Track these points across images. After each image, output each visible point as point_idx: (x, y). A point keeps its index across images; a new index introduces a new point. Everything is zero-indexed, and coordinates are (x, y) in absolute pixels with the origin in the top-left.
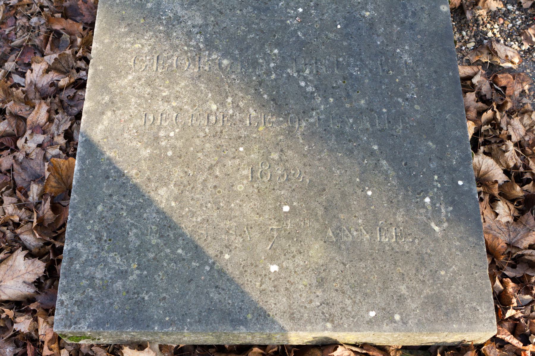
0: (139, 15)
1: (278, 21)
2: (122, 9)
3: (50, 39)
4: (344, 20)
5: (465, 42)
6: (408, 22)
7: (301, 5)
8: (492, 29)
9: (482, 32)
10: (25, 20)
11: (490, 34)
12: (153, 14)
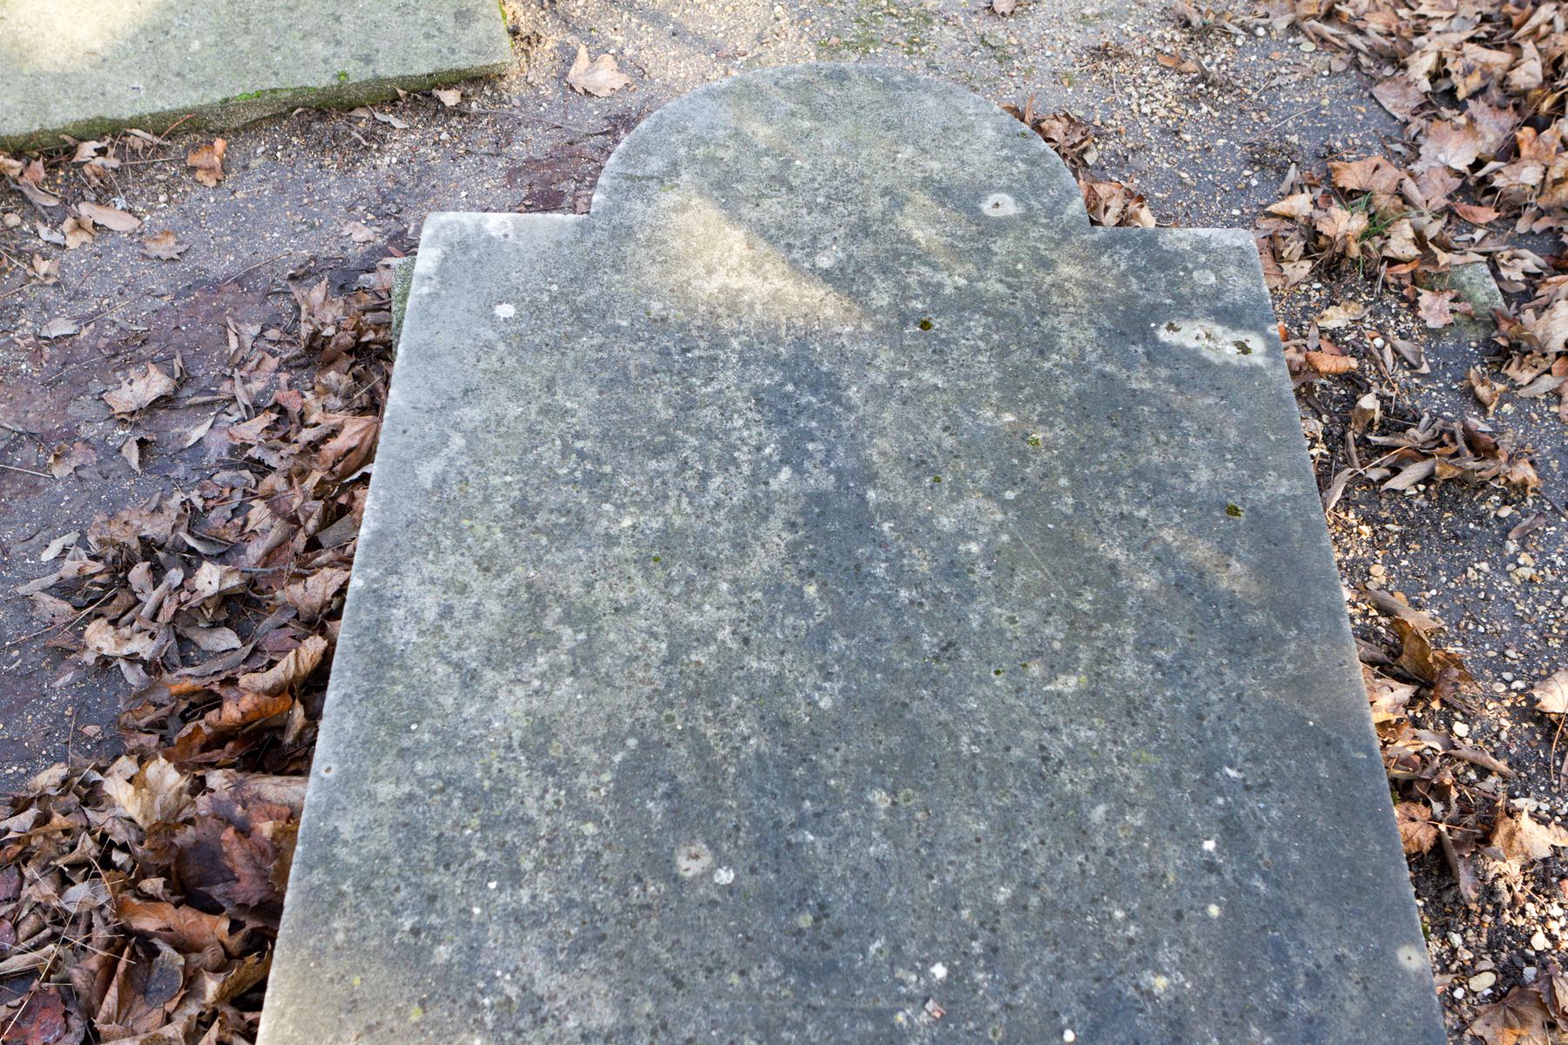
0: (406, 990)
1: (869, 1015)
2: (354, 969)
3: (121, 967)
4: (1083, 1008)
5: (1462, 969)
6: (1298, 1013)
7: (941, 952)
8: (1543, 921)
9: (1512, 930)
10: (47, 888)
11: (1540, 942)
12: (453, 988)
